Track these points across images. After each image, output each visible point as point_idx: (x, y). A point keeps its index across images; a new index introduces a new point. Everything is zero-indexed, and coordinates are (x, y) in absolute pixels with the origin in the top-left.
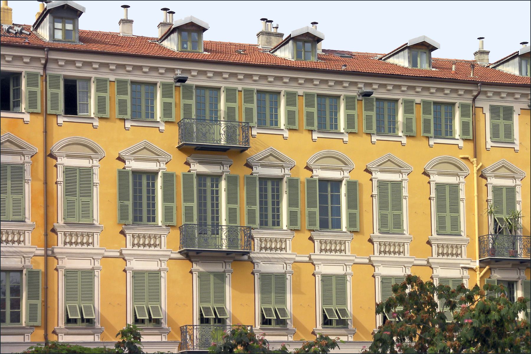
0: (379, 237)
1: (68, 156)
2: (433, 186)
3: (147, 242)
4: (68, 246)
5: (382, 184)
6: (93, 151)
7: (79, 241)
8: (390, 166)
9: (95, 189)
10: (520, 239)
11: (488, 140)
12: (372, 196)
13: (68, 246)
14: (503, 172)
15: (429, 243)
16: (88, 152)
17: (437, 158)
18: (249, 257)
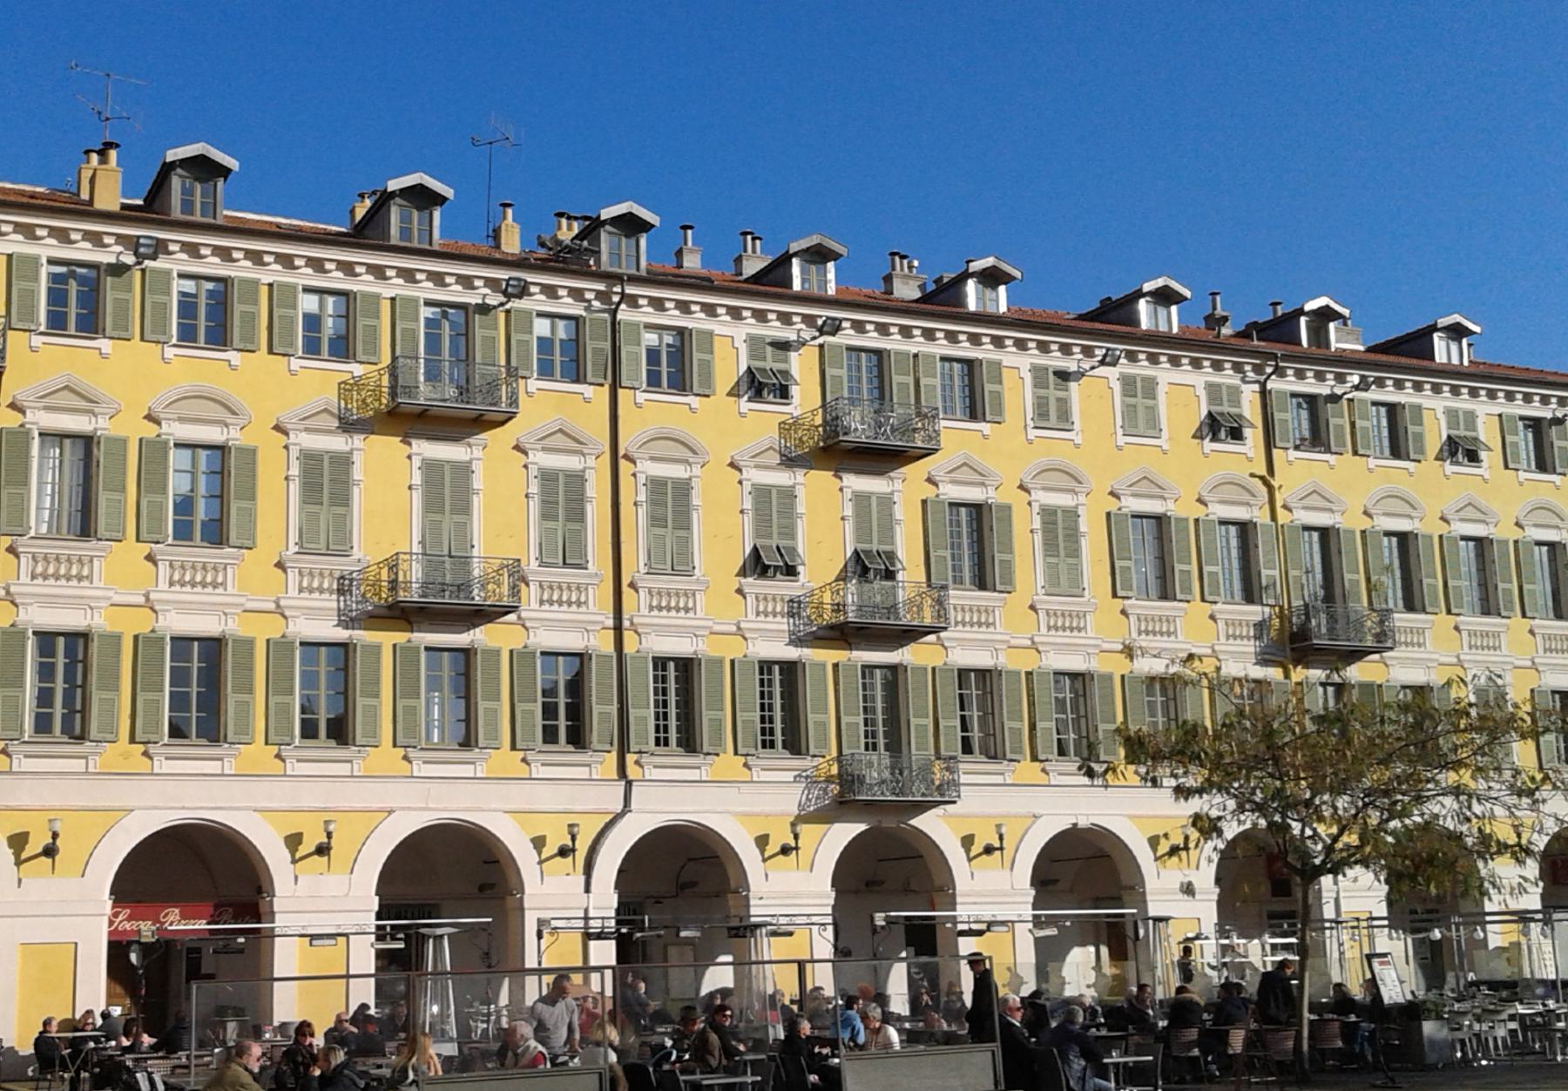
0: (537, 573)
1: (181, 420)
2: (416, 462)
3: (74, 572)
4: (177, 588)
5: (1048, 514)
6: (689, 450)
7: (673, 604)
8: (560, 441)
9: (475, 498)
10: (904, 588)
11: (1120, 431)
12: (410, 488)
13: (40, 581)
14: (1315, 501)
15: (1032, 607)
16: (683, 453)
17: (1044, 460)
18: (519, 617)
